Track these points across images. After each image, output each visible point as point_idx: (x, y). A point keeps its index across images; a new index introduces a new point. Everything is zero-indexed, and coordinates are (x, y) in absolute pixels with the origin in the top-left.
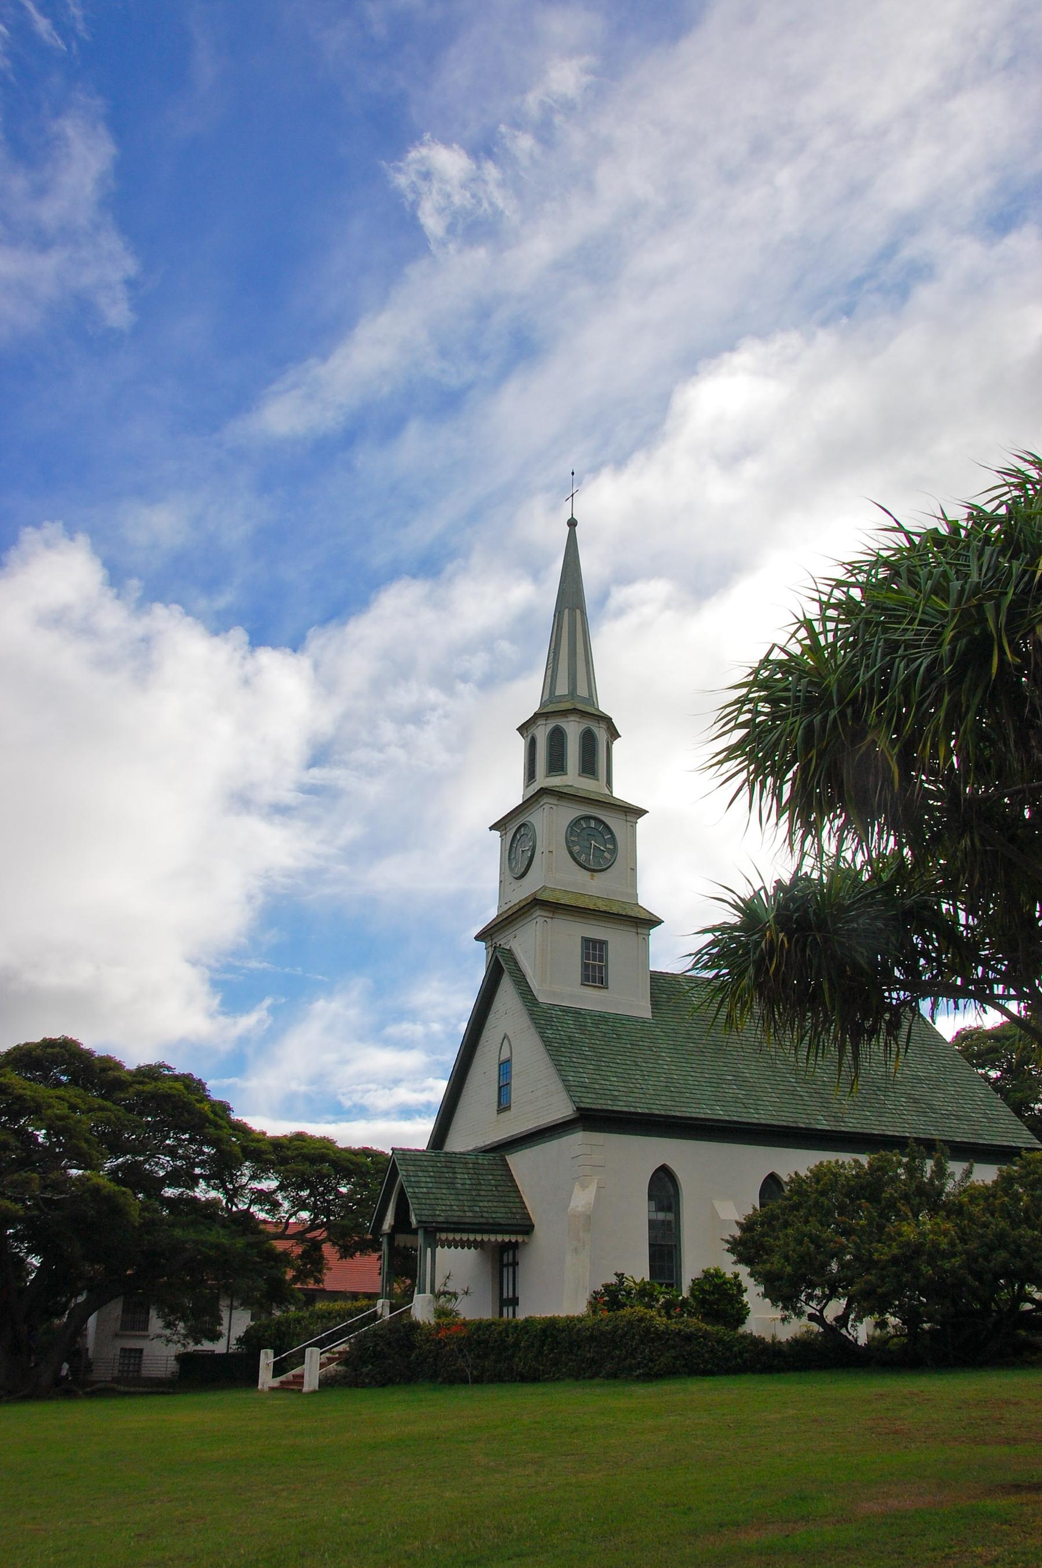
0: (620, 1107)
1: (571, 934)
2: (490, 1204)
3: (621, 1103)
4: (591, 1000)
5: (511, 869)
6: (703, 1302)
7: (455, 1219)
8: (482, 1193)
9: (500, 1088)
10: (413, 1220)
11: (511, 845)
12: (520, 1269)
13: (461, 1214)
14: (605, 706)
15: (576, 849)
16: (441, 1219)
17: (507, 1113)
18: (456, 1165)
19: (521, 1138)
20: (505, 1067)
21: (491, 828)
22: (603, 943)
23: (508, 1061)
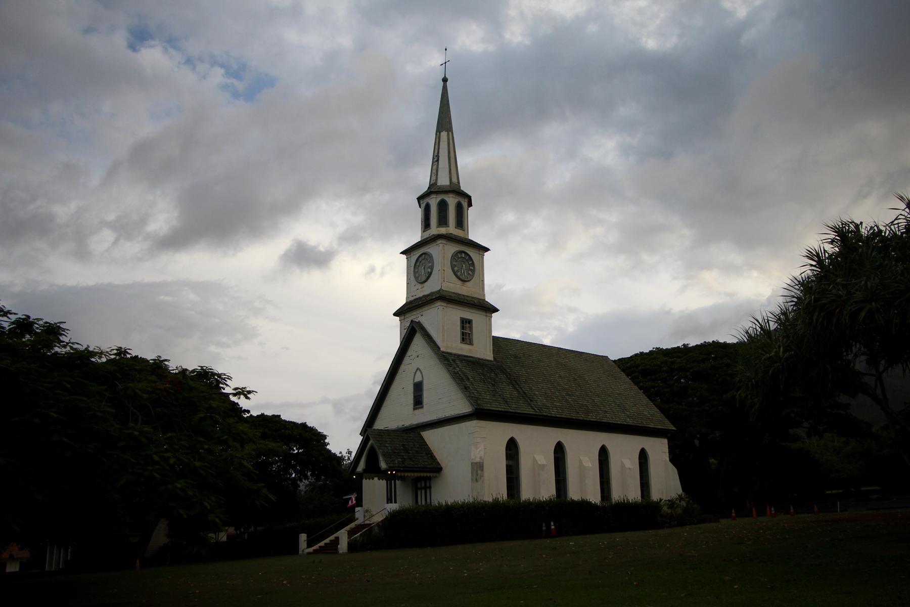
1: (456, 314)
4: (464, 350)
5: (417, 278)
10: (383, 465)
12: (433, 489)
15: (456, 269)
20: (418, 387)
22: (470, 322)
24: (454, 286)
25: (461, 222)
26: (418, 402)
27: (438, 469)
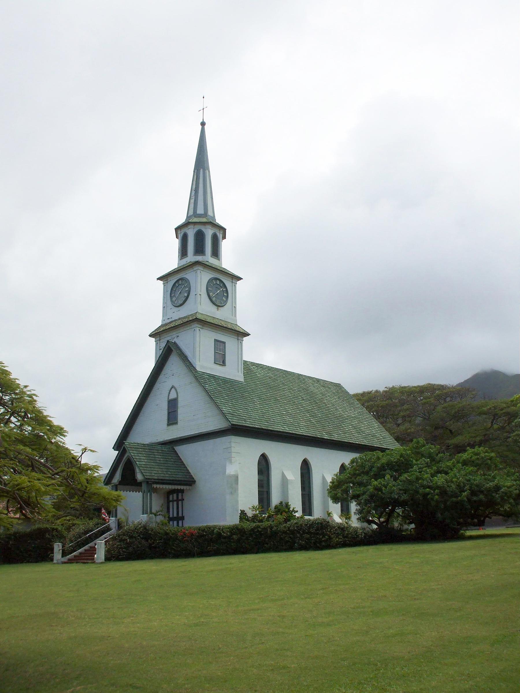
0: (248, 424)
2: (174, 471)
3: (248, 423)
4: (218, 371)
6: (378, 503)
10: (139, 477)
11: (172, 289)
12: (185, 502)
13: (164, 475)
14: (220, 220)
15: (211, 294)
16: (156, 478)
18: (154, 451)
21: (158, 279)
25: (216, 253)
26: (172, 418)
27: (191, 482)
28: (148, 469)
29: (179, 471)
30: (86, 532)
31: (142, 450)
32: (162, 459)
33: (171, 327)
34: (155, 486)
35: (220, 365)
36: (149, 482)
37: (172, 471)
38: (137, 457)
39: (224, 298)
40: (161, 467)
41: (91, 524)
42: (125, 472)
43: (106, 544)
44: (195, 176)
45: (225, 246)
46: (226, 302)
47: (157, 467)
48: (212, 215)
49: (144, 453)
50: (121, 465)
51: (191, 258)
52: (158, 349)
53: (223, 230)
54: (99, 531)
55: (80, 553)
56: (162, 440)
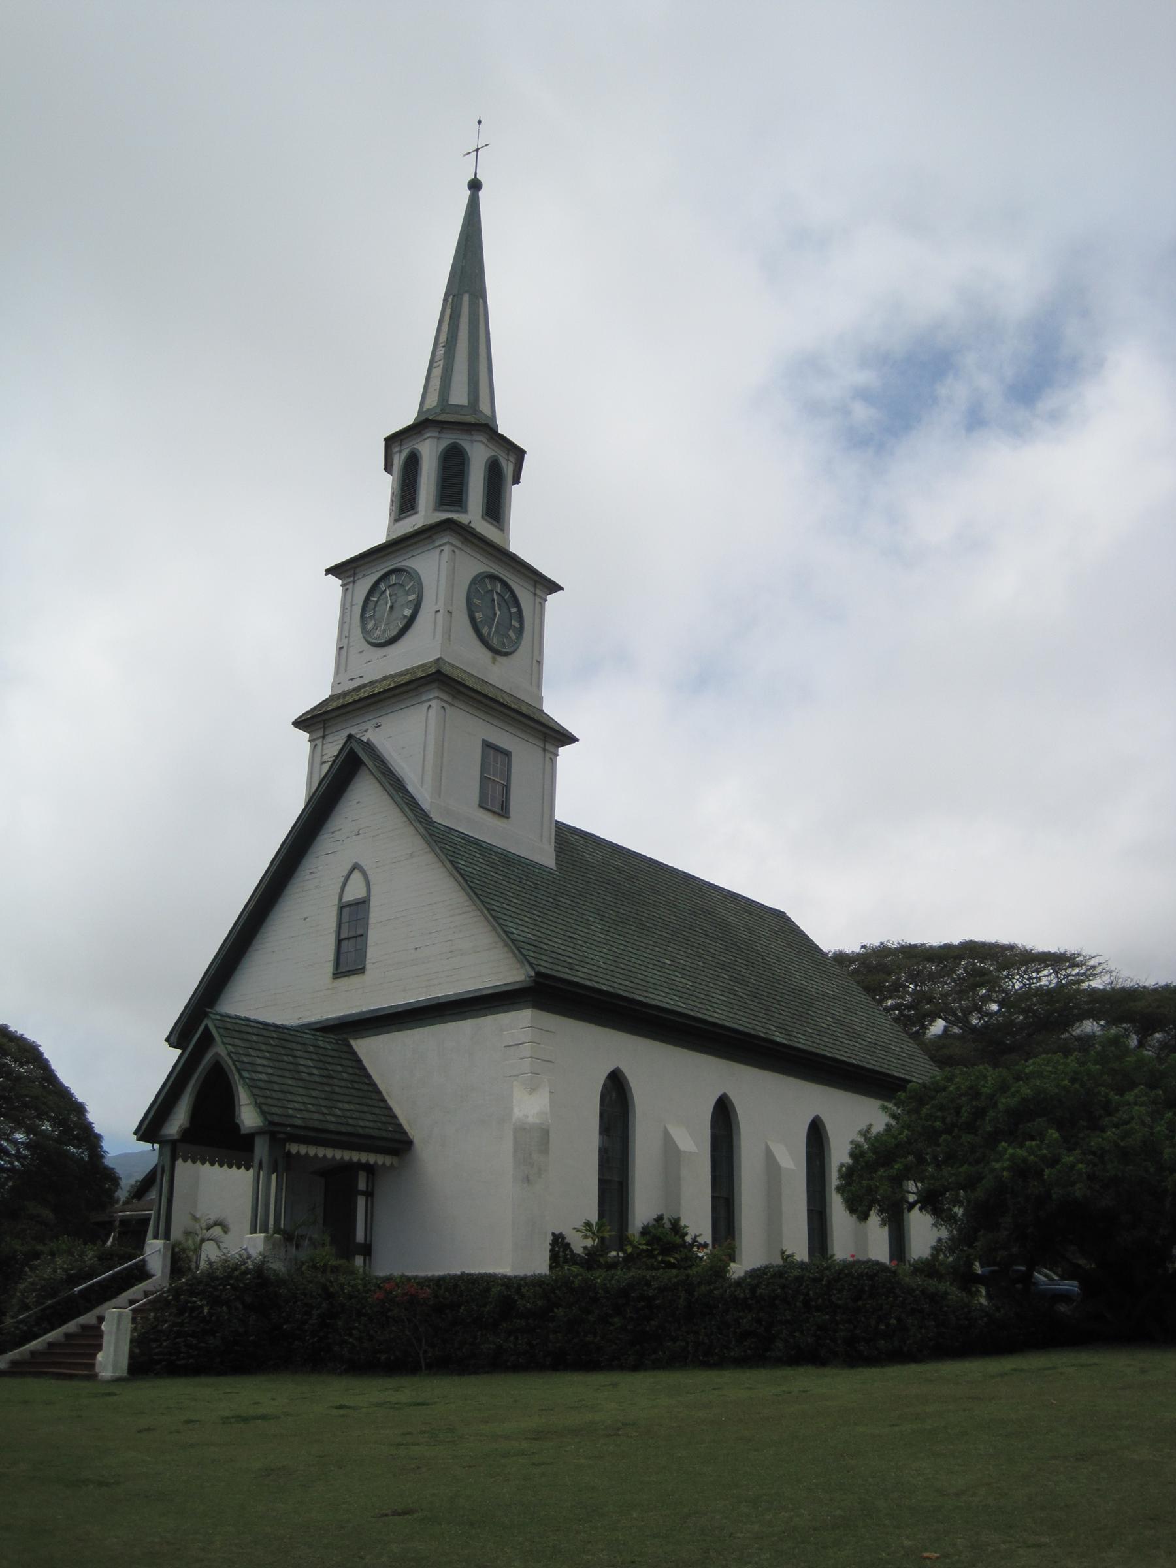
0: (580, 976)
1: (473, 730)
3: (579, 974)
7: (316, 1124)
8: (337, 1090)
9: (339, 942)
10: (249, 1117)
13: (321, 1117)
15: (479, 616)
16: (299, 1122)
17: (355, 980)
18: (294, 1046)
19: (381, 1016)
21: (329, 571)
23: (362, 905)
24: (471, 659)
25: (496, 509)
26: (348, 960)
27: (398, 1144)
28: (274, 1095)
29: (365, 1109)
30: (73, 1280)
31: (261, 1039)
32: (315, 1071)
33: (361, 700)
34: (294, 1148)
35: (494, 813)
36: (277, 1133)
37: (347, 1106)
38: (245, 1059)
39: (511, 633)
40: (314, 1093)
41: (91, 1255)
42: (201, 1106)
43: (134, 1320)
44: (448, 311)
45: (519, 497)
46: (516, 644)
47: (301, 1091)
48: (488, 412)
49: (263, 1047)
50: (196, 1076)
51: (425, 513)
52: (318, 760)
53: (518, 454)
54: (112, 1276)
55: (51, 1345)
56: (313, 1019)
